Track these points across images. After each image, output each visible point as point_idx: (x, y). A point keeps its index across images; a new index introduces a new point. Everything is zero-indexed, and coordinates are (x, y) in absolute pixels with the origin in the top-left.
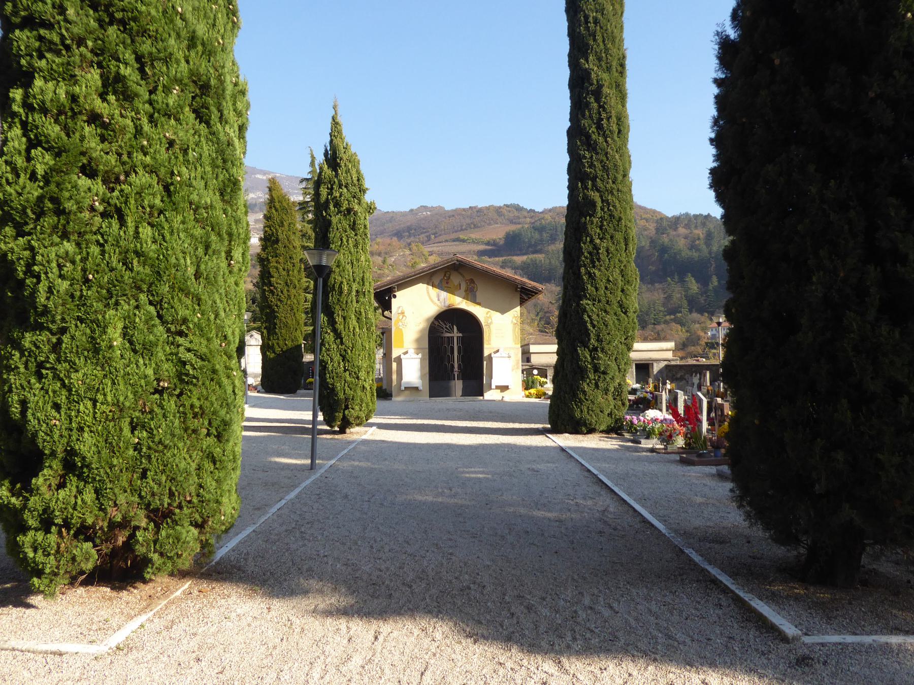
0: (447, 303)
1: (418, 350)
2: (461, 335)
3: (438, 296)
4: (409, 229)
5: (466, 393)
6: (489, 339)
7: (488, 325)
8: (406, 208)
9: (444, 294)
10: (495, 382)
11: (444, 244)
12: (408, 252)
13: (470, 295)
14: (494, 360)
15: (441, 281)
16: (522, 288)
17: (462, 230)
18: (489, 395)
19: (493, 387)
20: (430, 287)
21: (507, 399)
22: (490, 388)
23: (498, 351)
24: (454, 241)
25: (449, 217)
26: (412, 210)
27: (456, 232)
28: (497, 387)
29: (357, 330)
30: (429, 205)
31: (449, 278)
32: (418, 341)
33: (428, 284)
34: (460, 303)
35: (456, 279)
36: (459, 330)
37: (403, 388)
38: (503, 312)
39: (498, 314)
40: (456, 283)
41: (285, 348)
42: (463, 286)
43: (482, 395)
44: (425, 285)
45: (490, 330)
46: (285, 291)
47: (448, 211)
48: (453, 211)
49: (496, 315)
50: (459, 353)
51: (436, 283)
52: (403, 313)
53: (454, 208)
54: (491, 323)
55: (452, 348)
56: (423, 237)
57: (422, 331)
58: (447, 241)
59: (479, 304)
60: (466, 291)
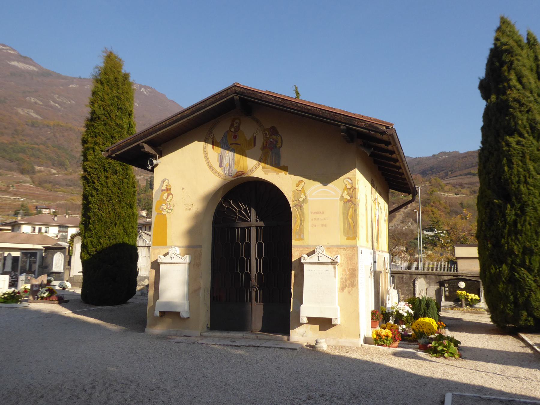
0: (235, 169)
1: (191, 249)
2: (262, 224)
3: (221, 160)
4: (432, 169)
5: (266, 329)
6: (301, 231)
7: (300, 205)
8: (430, 154)
9: (229, 156)
10: (308, 310)
11: (458, 177)
12: (428, 184)
13: (272, 156)
14: (306, 267)
15: (226, 136)
16: (348, 131)
17: (472, 167)
18: (302, 335)
19: (304, 320)
20: (210, 146)
21: (324, 347)
22: (300, 324)
23: (313, 252)
24: (466, 175)
25: (463, 158)
26: (434, 156)
27: (468, 168)
28: (312, 321)
29: (102, 214)
30: (448, 151)
31: (238, 129)
32: (192, 233)
33: (206, 141)
34: (257, 169)
35: (248, 130)
36: (261, 216)
37: (157, 313)
38: (326, 180)
39: (318, 185)
40: (248, 136)
41: (99, 248)
42: (260, 142)
43: (288, 334)
44: (202, 144)
45: (302, 214)
46: (103, 178)
47: (461, 154)
48: (465, 153)
49: (314, 190)
50: (260, 255)
51: (218, 139)
52: (168, 190)
53: (466, 151)
54: (305, 201)
55: (249, 246)
56: (442, 174)
57: (198, 218)
58: (460, 175)
59: (284, 169)
60: (264, 148)
